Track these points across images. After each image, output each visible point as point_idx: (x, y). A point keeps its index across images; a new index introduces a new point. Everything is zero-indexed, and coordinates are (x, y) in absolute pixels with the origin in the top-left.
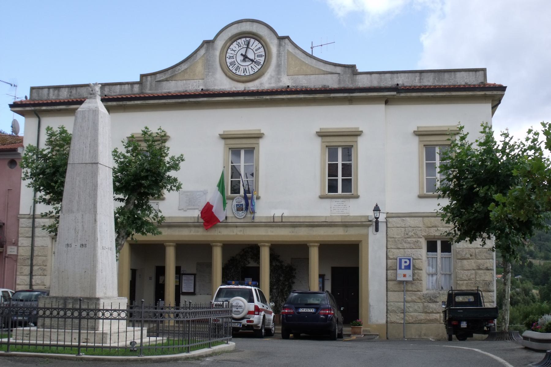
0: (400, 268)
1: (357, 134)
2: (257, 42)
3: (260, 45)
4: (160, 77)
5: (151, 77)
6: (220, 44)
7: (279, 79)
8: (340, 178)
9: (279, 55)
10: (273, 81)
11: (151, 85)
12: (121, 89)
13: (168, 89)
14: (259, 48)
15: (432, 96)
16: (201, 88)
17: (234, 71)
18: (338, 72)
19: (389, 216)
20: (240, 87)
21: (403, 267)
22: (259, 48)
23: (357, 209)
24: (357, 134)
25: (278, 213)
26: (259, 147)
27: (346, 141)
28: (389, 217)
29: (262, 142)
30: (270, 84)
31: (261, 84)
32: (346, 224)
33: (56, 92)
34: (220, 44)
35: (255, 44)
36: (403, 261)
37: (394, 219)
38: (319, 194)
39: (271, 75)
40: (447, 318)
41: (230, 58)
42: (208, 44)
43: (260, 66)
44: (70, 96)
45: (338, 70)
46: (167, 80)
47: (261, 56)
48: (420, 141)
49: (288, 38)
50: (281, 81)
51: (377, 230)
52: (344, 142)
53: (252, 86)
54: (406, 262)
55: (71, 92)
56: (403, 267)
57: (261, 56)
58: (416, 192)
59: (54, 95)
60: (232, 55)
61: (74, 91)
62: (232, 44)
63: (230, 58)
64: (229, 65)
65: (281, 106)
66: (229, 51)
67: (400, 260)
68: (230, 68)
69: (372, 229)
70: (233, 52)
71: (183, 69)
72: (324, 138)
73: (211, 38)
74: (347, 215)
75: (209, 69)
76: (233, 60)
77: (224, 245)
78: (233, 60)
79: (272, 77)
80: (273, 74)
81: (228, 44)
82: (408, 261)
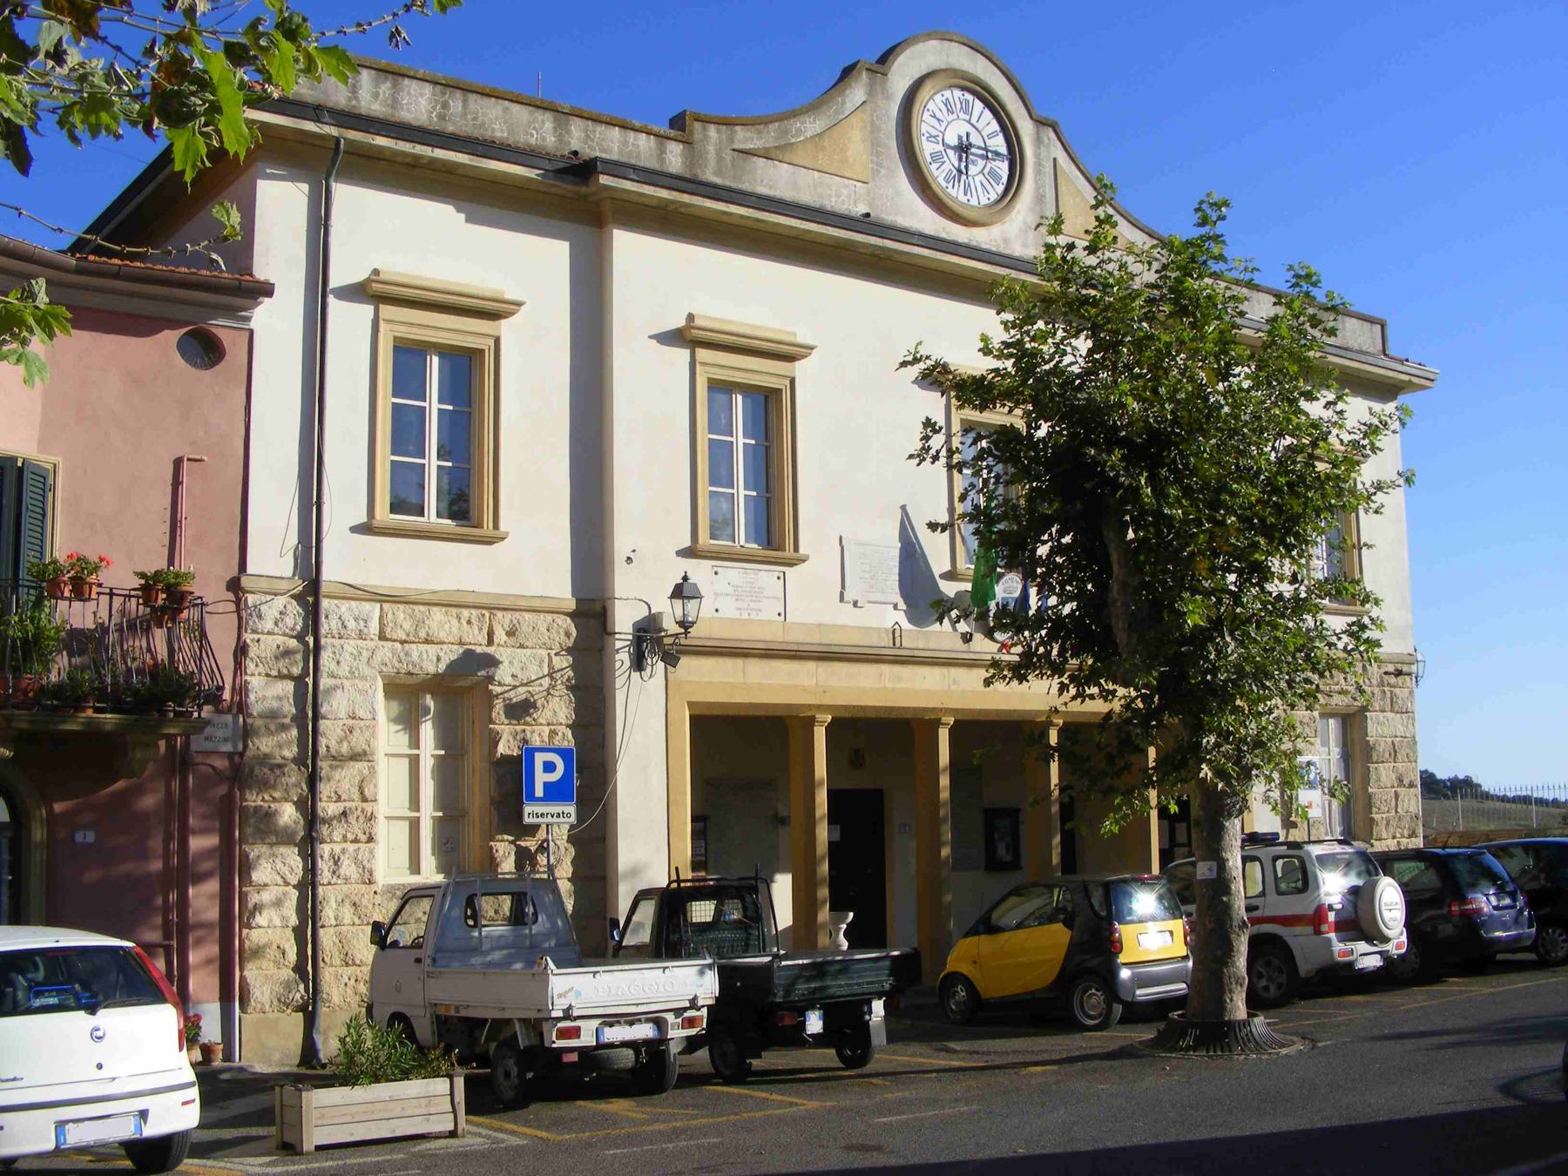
4: (746, 140)
5: (718, 131)
11: (720, 159)
12: (626, 143)
13: (602, 150)
15: (663, 205)
21: (539, 792)
27: (762, 372)
30: (1025, 246)
31: (1006, 240)
33: (386, 87)
36: (540, 759)
40: (273, 873)
44: (442, 117)
46: (766, 155)
55: (445, 105)
56: (539, 792)
59: (376, 96)
60: (934, 133)
61: (456, 104)
71: (809, 134)
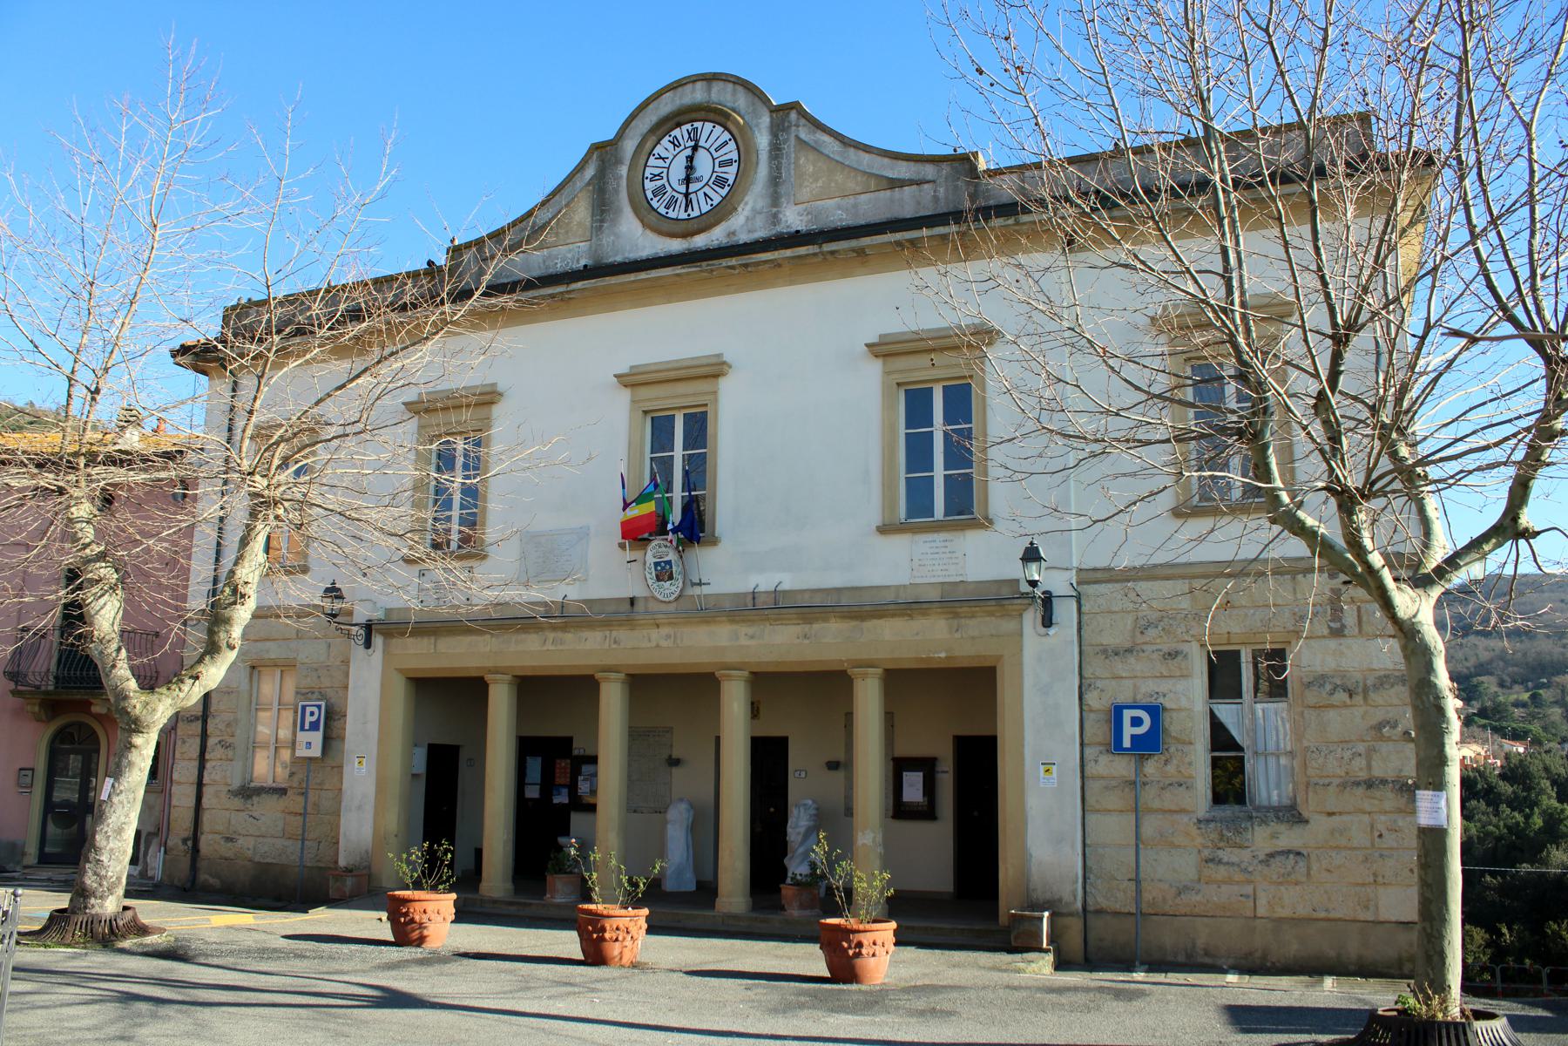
0: (302, 729)
1: (714, 370)
2: (719, 129)
3: (727, 136)
6: (629, 146)
7: (775, 216)
8: (939, 472)
9: (776, 150)
10: (759, 221)
14: (726, 143)
16: (583, 262)
17: (662, 210)
18: (930, 177)
19: (1089, 577)
20: (676, 246)
22: (726, 143)
23: (981, 557)
24: (714, 370)
25: (764, 582)
26: (716, 401)
27: (947, 367)
28: (1088, 583)
29: (726, 385)
32: (958, 602)
34: (629, 146)
35: (711, 133)
36: (1128, 715)
37: (1103, 588)
38: (876, 519)
39: (753, 210)
41: (654, 177)
42: (604, 152)
43: (727, 189)
45: (929, 171)
47: (729, 163)
48: (887, 373)
49: (795, 106)
50: (779, 221)
51: (1047, 621)
52: (657, 399)
53: (700, 241)
54: (312, 714)
57: (729, 163)
58: (875, 517)
60: (657, 171)
62: (658, 142)
63: (654, 177)
64: (650, 195)
65: (773, 285)
66: (652, 162)
67: (1118, 711)
68: (654, 204)
69: (1032, 618)
70: (660, 163)
72: (890, 360)
73: (610, 135)
74: (958, 579)
75: (603, 212)
76: (659, 183)
77: (887, 671)
78: (659, 183)
79: (755, 212)
80: (762, 203)
81: (649, 145)
82: (315, 710)
